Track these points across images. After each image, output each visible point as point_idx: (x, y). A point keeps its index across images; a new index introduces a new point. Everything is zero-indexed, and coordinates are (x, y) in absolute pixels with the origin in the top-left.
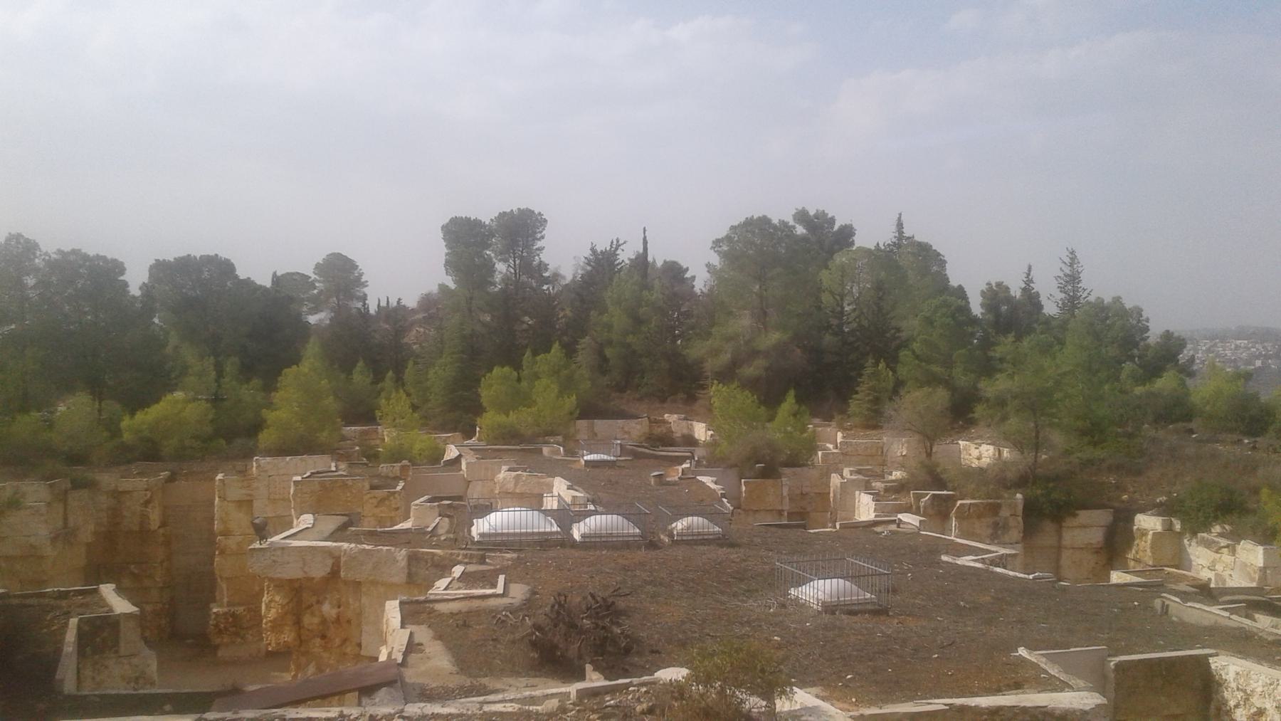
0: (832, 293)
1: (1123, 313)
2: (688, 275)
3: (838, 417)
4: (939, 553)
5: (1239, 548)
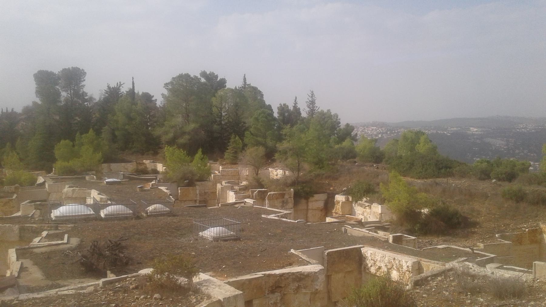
1: (330, 117)
2: (153, 99)
3: (220, 160)
5: (372, 206)
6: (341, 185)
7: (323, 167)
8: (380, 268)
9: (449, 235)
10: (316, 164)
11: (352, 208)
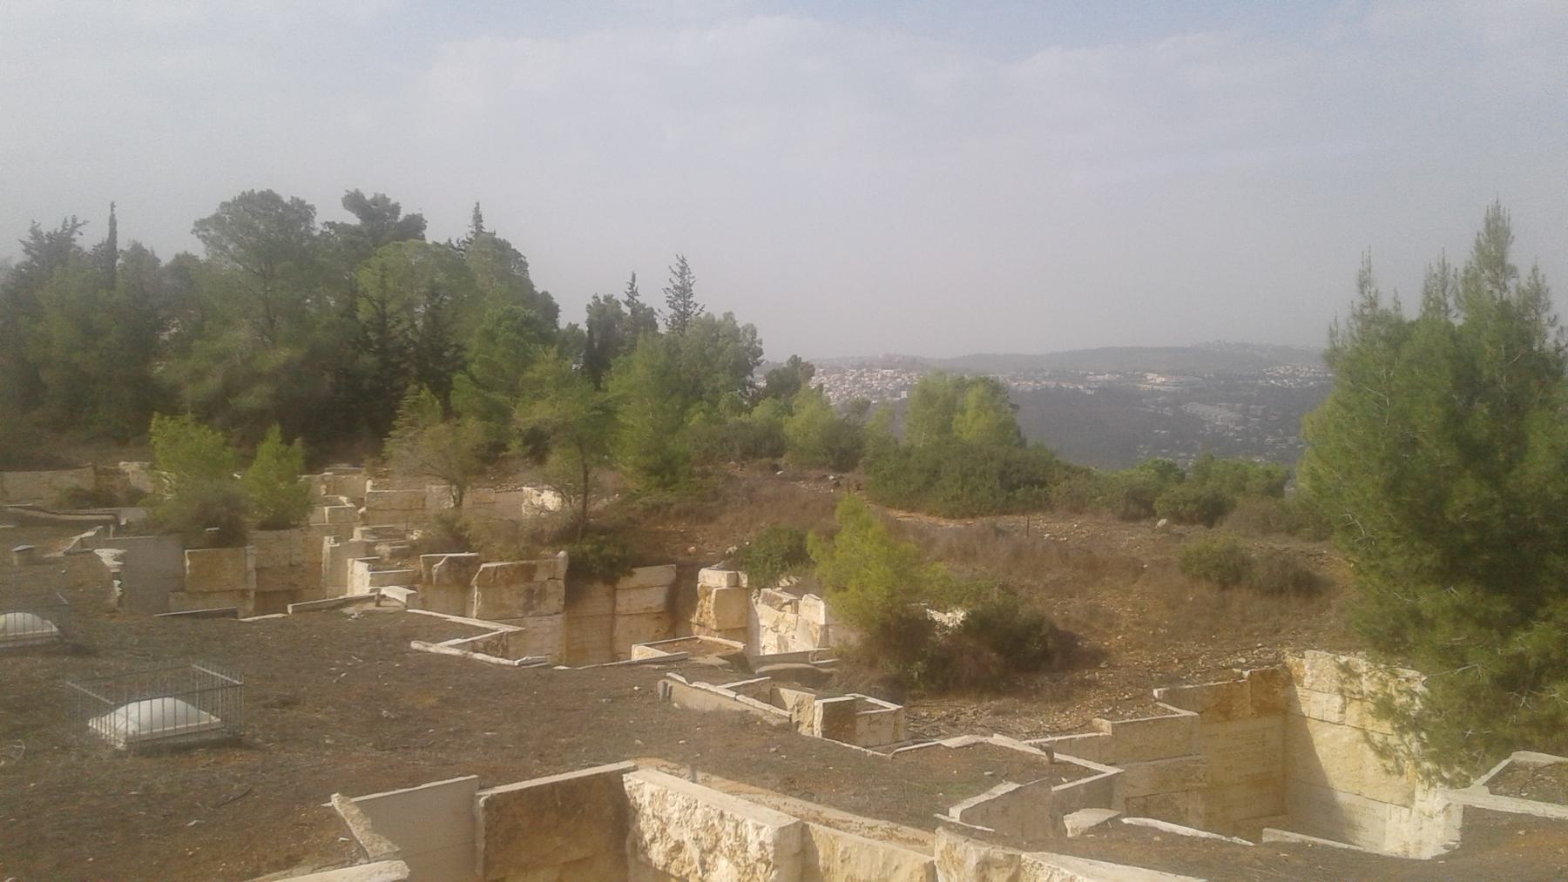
0: (370, 299)
1: (734, 334)
3: (369, 461)
4: (408, 638)
5: (801, 603)
6: (722, 537)
7: (675, 482)
8: (679, 847)
9: (1012, 690)
10: (653, 471)
11: (748, 612)
